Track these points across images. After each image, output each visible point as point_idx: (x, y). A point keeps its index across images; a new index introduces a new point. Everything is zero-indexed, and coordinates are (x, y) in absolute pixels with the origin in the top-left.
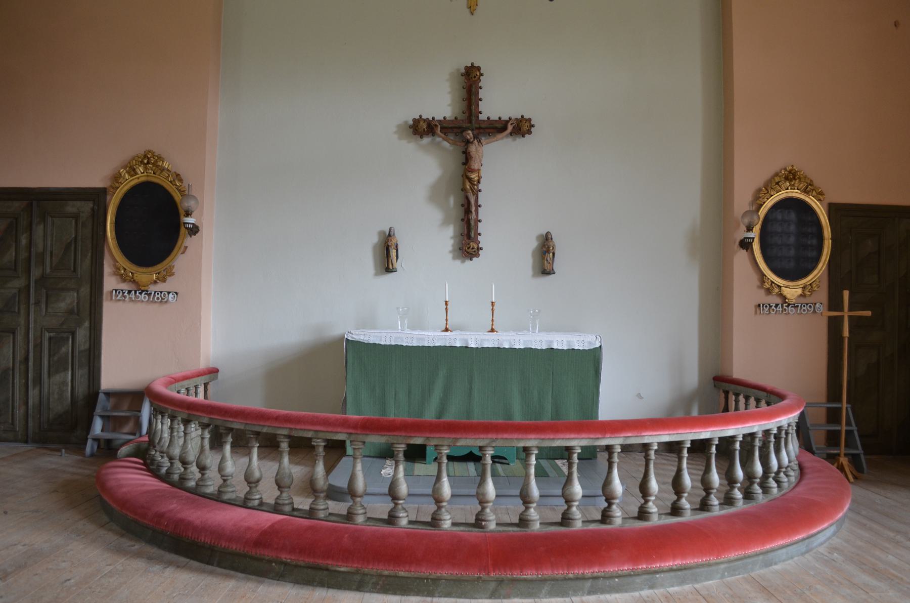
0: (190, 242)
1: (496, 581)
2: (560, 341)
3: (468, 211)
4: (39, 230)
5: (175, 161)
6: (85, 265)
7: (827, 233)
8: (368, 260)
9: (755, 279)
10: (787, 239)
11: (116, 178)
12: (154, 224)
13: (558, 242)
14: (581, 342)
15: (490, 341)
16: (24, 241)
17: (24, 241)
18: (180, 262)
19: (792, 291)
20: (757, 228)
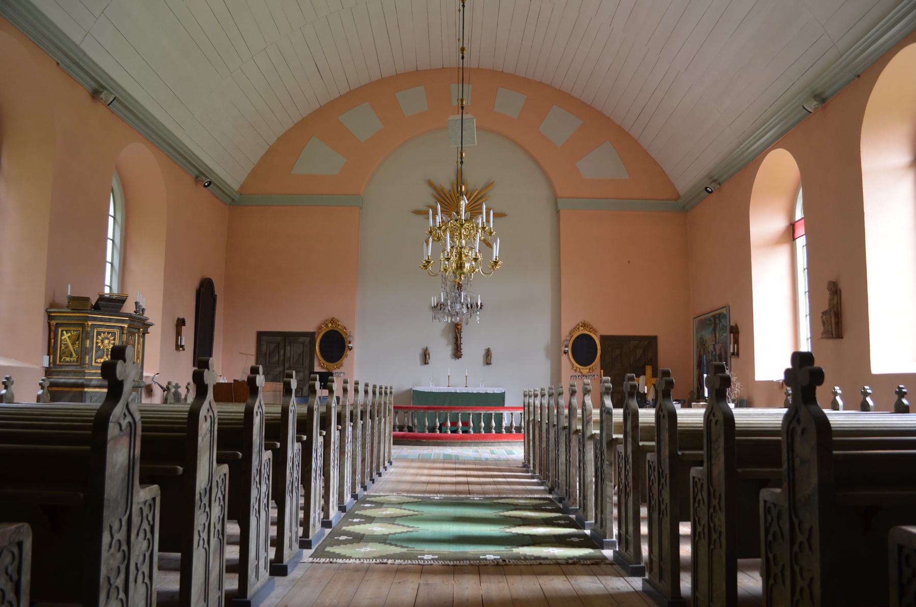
0: (349, 353)
1: (585, 394)
2: (490, 390)
3: (457, 340)
4: (288, 348)
5: (344, 322)
6: (307, 362)
7: (599, 347)
8: (418, 359)
9: (570, 365)
10: (583, 349)
11: (320, 328)
12: (335, 345)
13: (493, 351)
14: (497, 390)
15: (465, 390)
16: (282, 352)
17: (282, 352)
18: (345, 361)
19: (585, 370)
20: (570, 345)
